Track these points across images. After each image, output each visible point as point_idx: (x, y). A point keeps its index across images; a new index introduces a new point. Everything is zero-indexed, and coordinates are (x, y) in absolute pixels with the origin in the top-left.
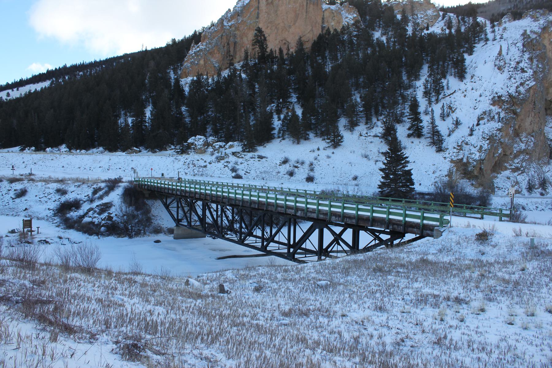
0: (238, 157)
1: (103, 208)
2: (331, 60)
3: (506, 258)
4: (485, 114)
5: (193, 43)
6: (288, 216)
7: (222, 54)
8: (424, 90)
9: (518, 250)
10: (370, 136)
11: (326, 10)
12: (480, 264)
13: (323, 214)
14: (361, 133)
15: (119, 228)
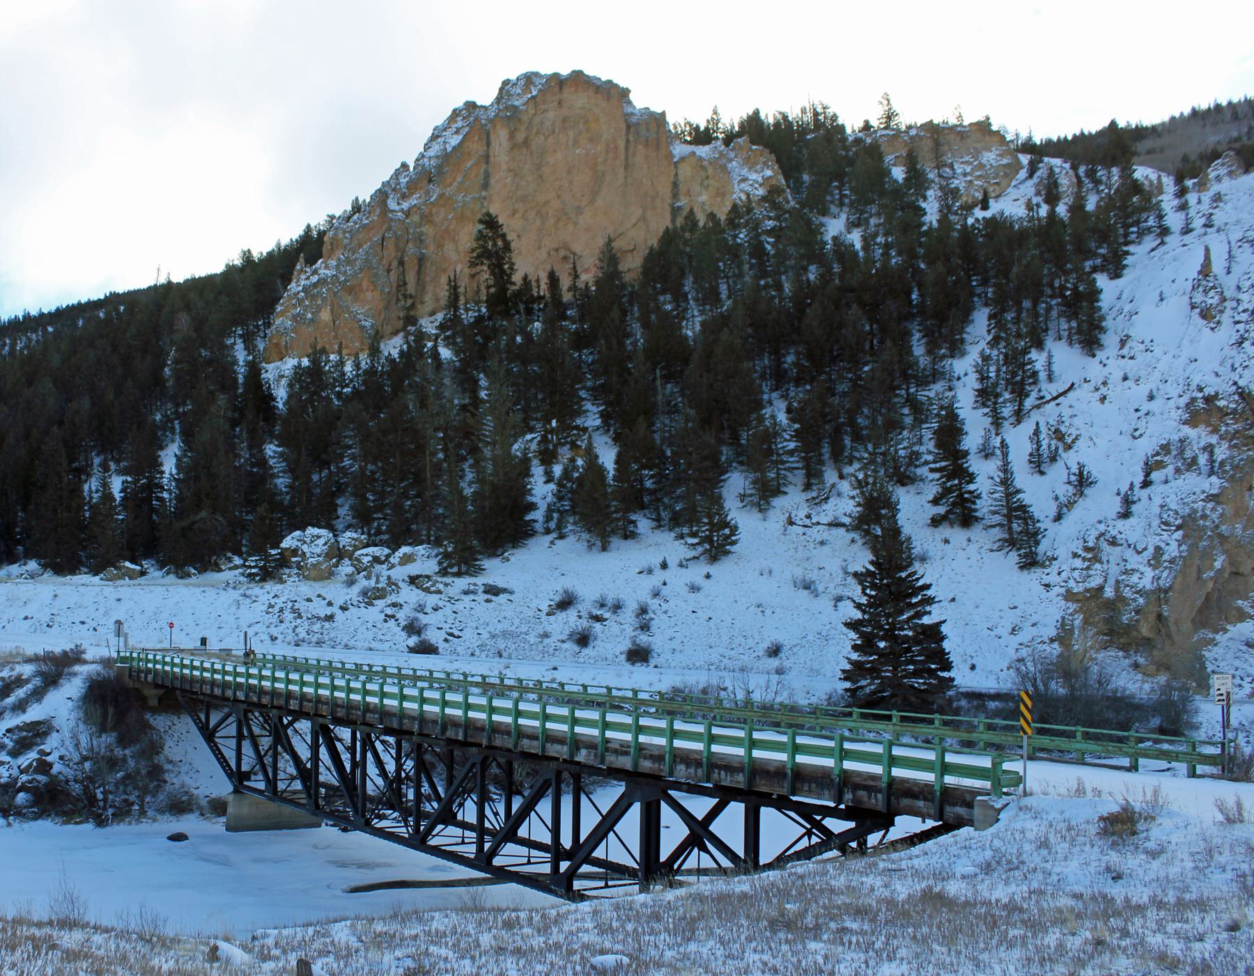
0: (427, 590)
1: (25, 738)
2: (702, 302)
3: (1186, 889)
4: (1168, 452)
5: (302, 260)
6: (553, 765)
7: (382, 292)
8: (978, 386)
9: (1229, 868)
10: (818, 523)
11: (683, 159)
12: (1106, 908)
13: (652, 757)
14: (790, 517)
15: (68, 795)
